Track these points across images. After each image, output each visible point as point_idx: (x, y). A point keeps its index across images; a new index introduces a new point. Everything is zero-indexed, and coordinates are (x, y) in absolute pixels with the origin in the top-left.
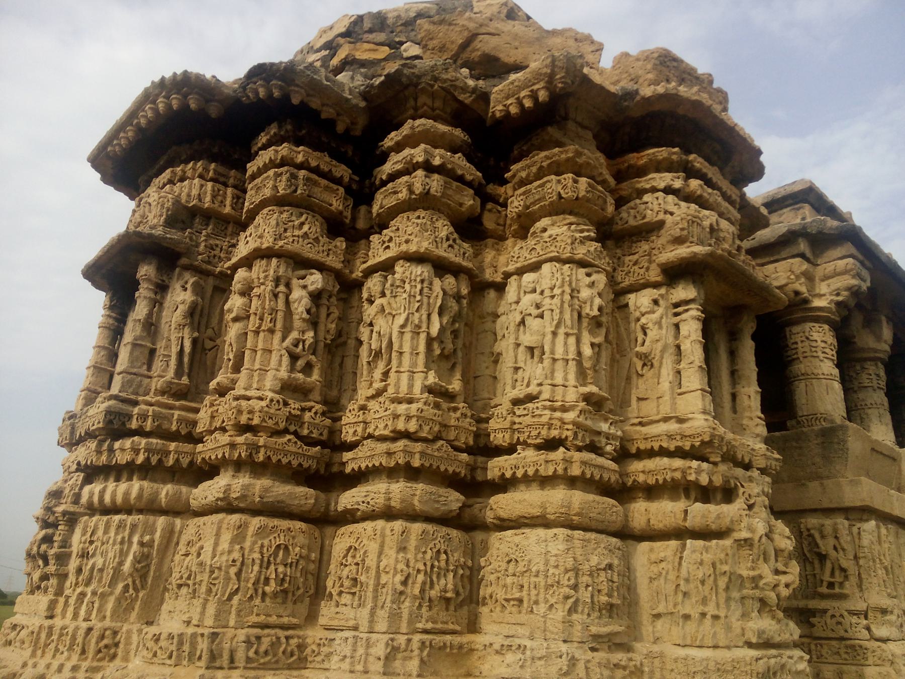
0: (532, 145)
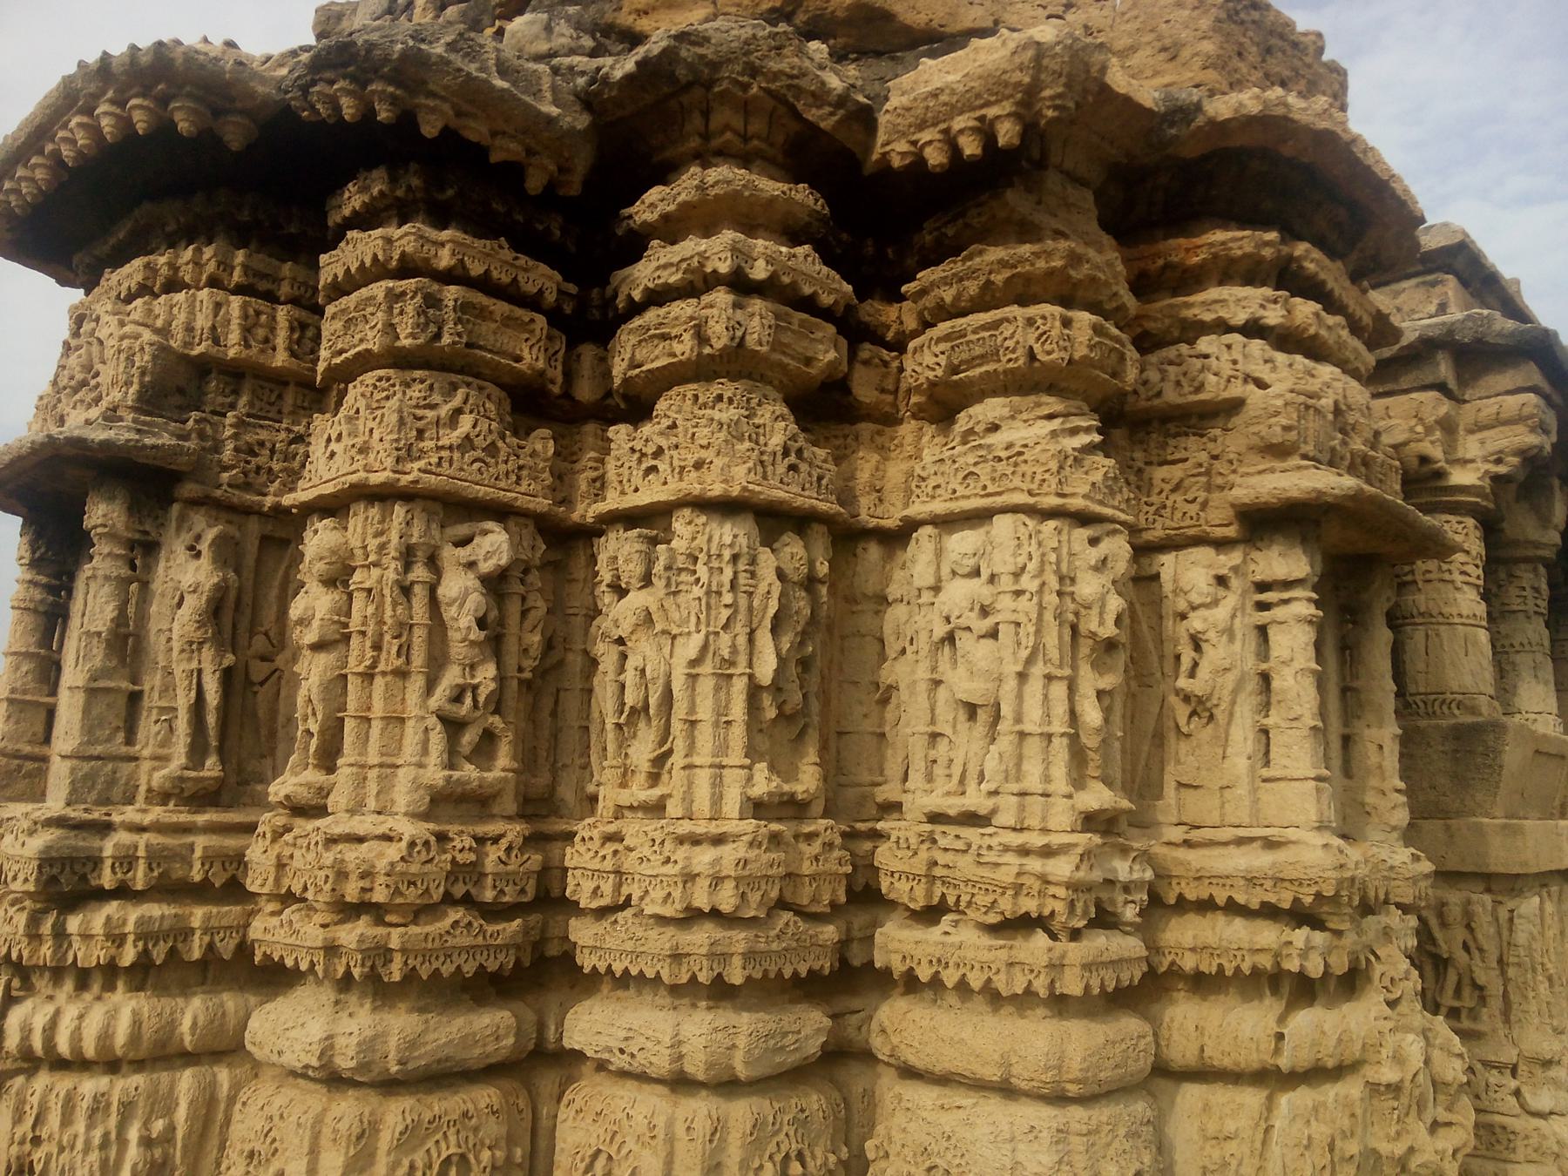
0: (967, 225)
